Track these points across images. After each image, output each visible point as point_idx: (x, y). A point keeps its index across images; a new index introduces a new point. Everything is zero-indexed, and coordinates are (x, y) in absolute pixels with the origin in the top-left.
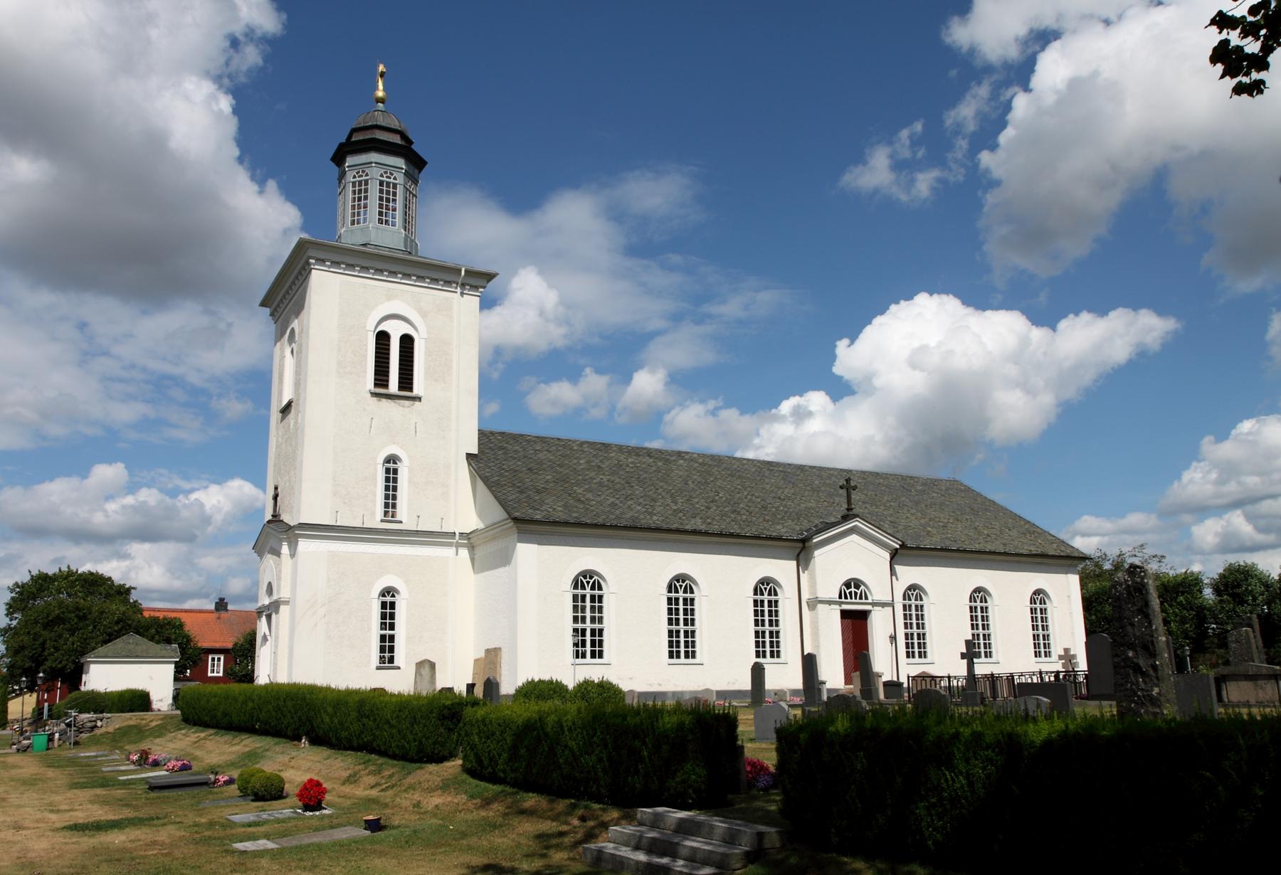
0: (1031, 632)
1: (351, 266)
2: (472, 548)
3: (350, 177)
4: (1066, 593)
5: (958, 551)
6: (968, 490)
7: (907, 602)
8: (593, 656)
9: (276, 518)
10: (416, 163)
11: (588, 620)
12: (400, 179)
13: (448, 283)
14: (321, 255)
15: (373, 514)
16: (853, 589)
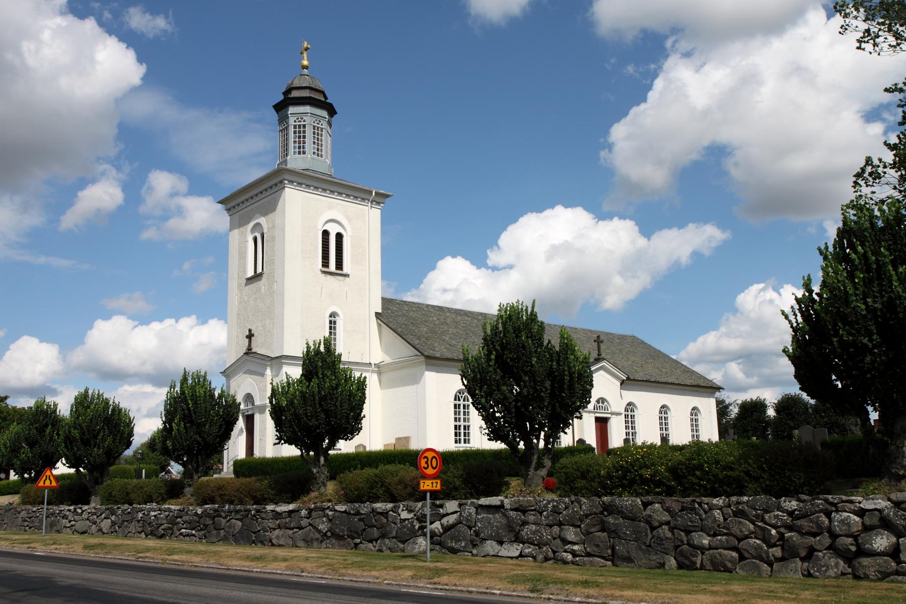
0: (453, 423)
2: (379, 373)
3: (292, 121)
4: (708, 407)
5: (654, 382)
6: (643, 343)
7: (457, 402)
9: (249, 352)
10: (332, 112)
12: (325, 125)
13: (363, 199)
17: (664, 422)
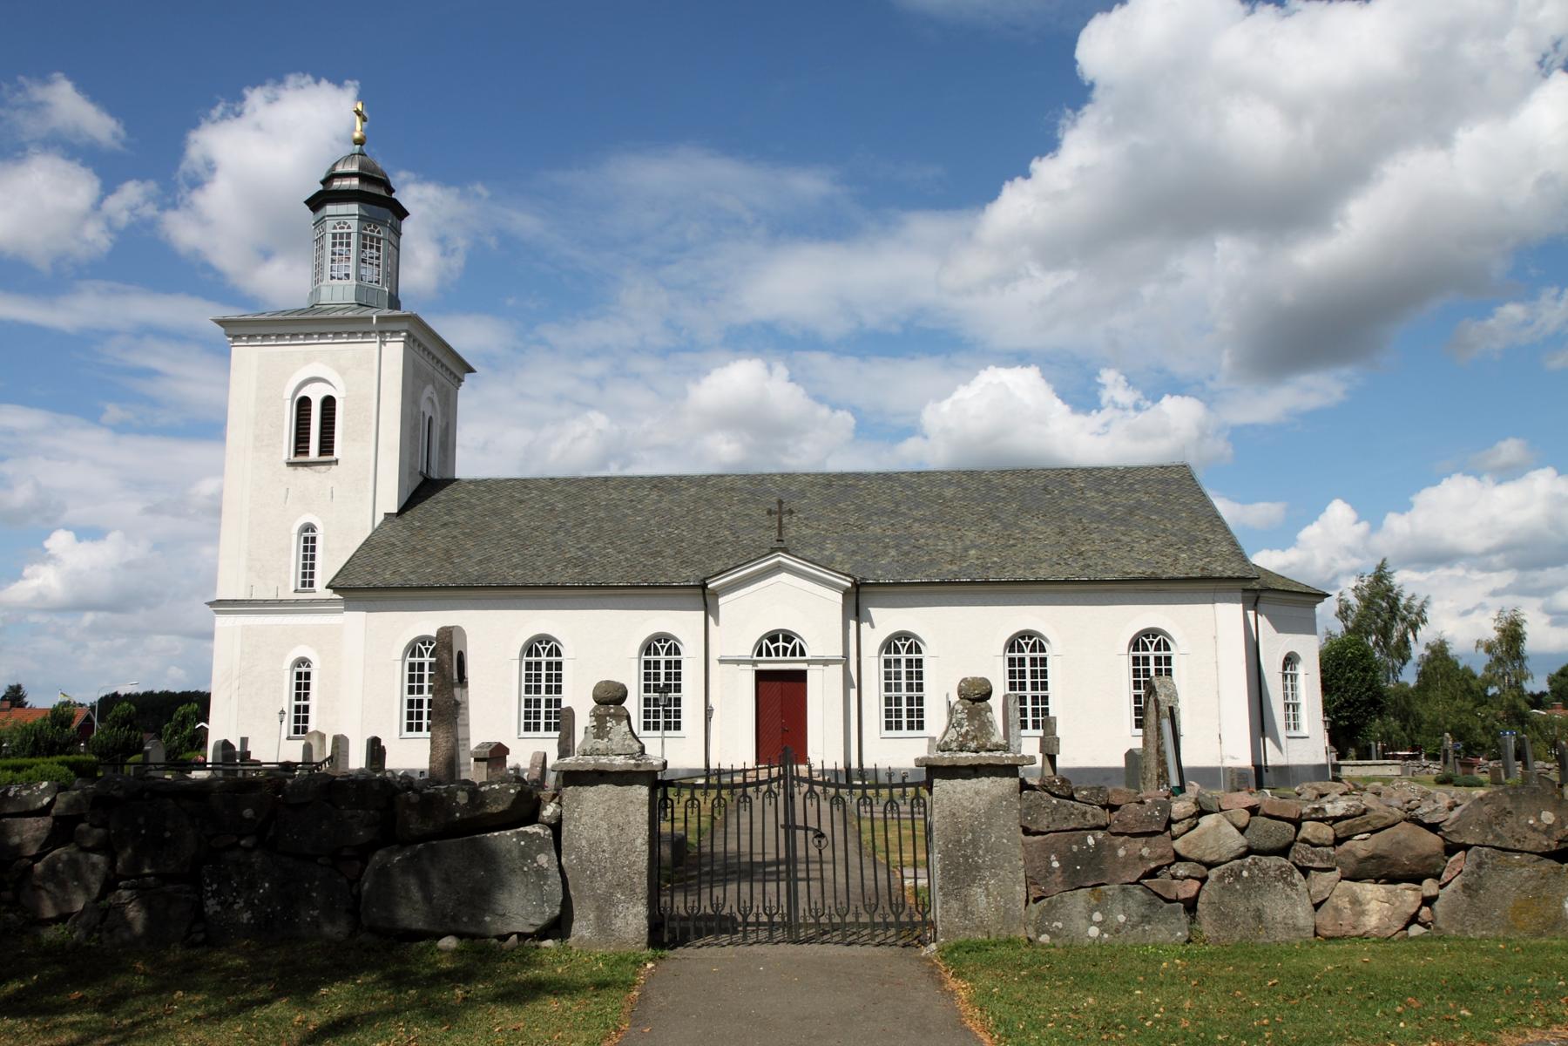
1: (265, 336)
8: (911, 727)
11: (1028, 686)
14: (252, 331)
15: (287, 585)
16: (781, 644)
17: (1153, 705)
